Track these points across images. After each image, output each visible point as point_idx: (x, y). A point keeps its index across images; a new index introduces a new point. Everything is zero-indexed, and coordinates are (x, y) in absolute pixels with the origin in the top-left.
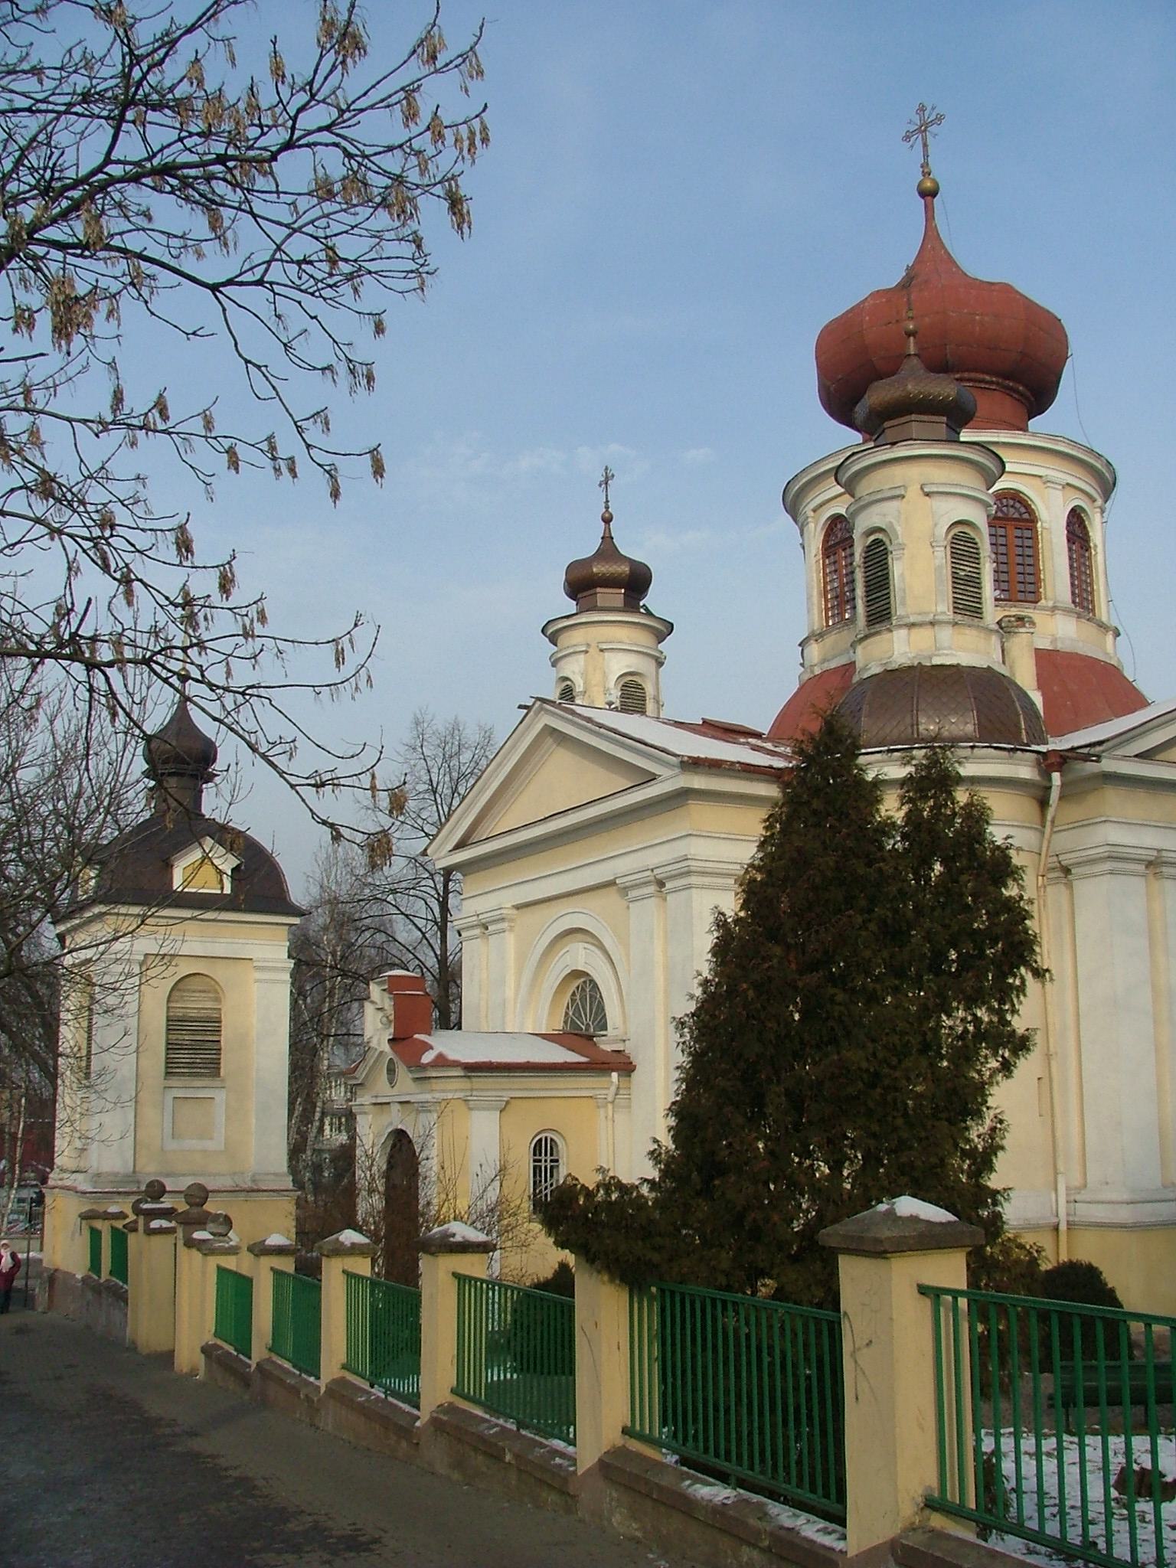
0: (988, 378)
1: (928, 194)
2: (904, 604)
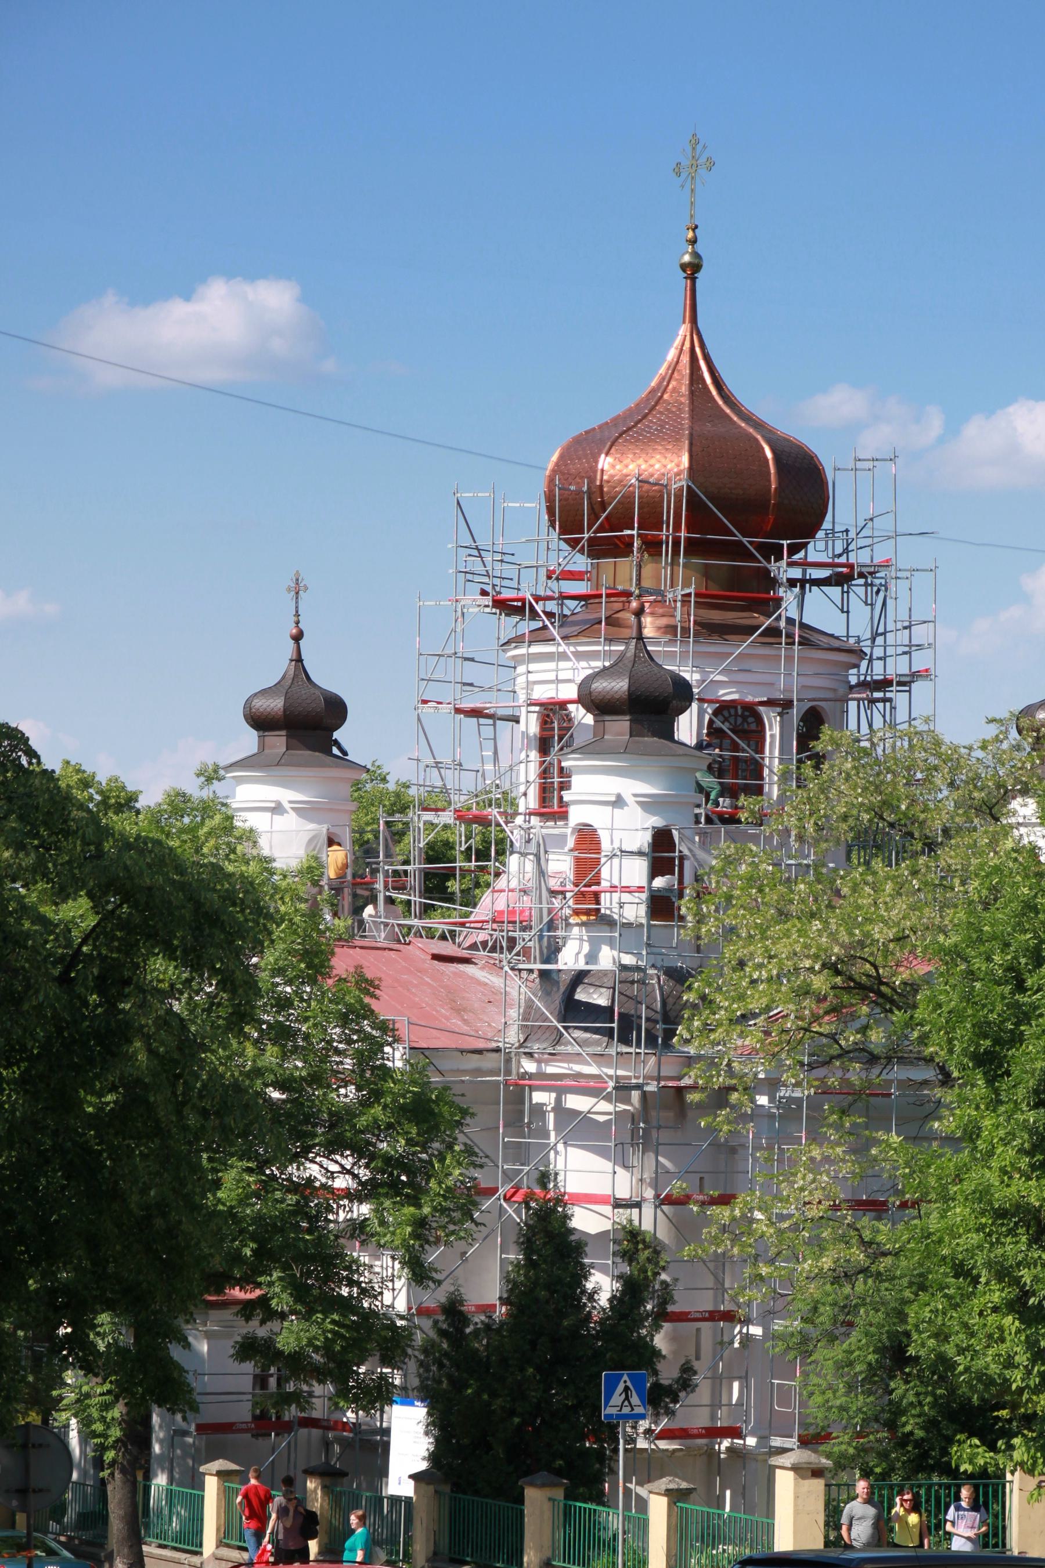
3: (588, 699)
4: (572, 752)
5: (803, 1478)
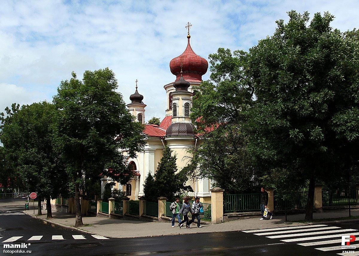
1: (189, 38)
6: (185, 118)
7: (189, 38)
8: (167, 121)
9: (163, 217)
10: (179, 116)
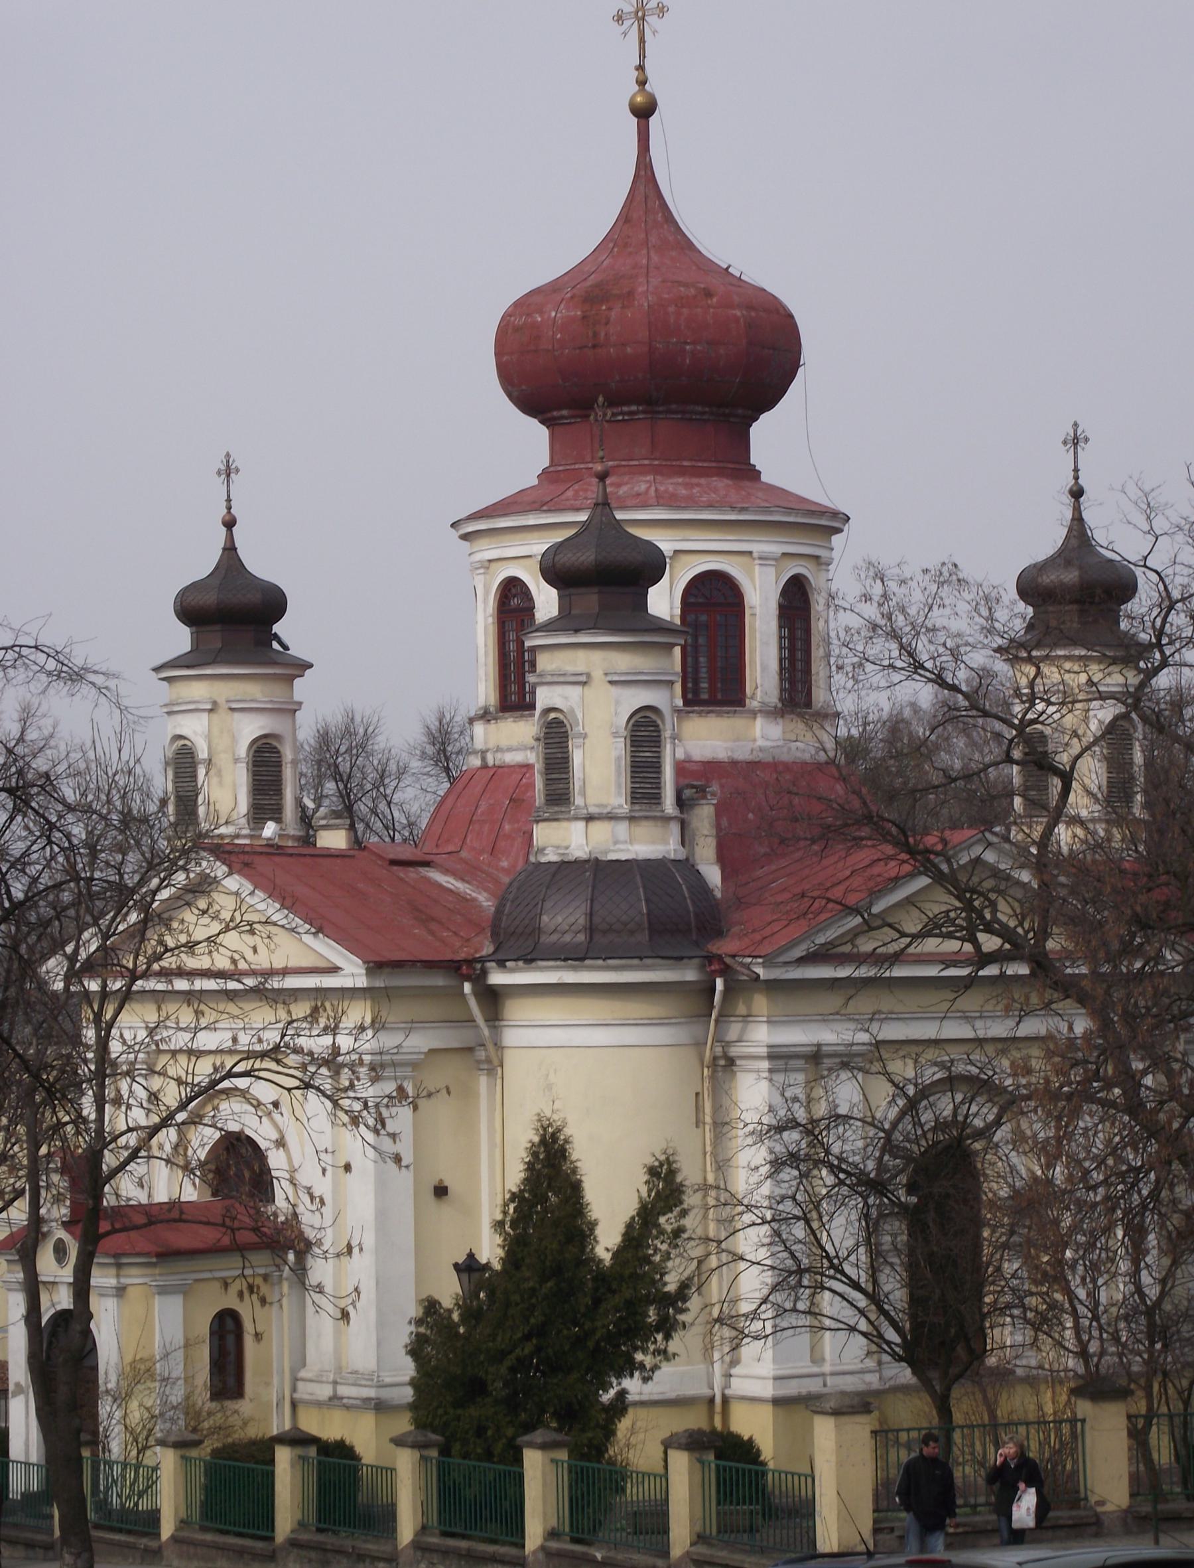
0: (699, 408)
1: (644, 112)
2: (584, 794)
3: (553, 573)
4: (536, 631)
5: (844, 1419)
6: (632, 819)
7: (644, 112)
8: (483, 806)
9: (554, 1545)
10: (592, 810)
